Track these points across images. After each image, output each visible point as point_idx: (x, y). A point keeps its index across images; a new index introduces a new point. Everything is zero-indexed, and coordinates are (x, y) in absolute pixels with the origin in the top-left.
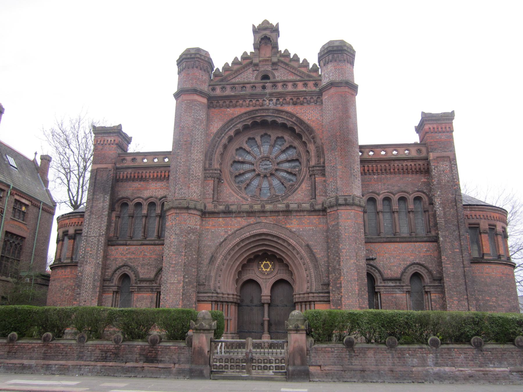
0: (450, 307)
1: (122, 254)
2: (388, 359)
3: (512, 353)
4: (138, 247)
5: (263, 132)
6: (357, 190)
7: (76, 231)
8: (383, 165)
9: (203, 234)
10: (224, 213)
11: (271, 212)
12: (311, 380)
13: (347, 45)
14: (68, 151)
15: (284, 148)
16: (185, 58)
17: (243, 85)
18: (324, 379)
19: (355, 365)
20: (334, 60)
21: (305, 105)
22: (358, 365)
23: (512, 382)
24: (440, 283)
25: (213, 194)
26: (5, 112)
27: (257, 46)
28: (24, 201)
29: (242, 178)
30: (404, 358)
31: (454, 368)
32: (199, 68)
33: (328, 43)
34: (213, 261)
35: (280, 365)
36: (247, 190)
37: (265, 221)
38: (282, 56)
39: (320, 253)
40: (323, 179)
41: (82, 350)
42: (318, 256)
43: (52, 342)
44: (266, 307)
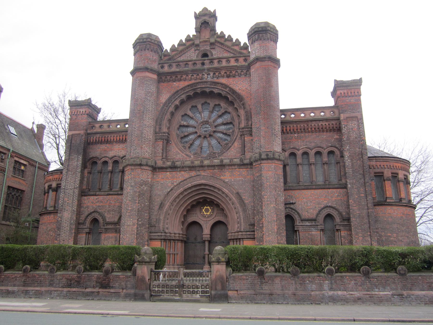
0: (356, 242)
1: (92, 202)
2: (291, 285)
3: (394, 280)
4: (105, 197)
5: (203, 101)
6: (278, 148)
7: (57, 185)
8: (302, 125)
9: (154, 185)
10: (171, 168)
11: (208, 166)
12: (229, 302)
13: (271, 26)
14: (57, 120)
15: (220, 113)
16: (139, 43)
17: (186, 63)
18: (239, 301)
19: (265, 290)
20: (259, 39)
21: (237, 77)
22: (267, 290)
23: (394, 304)
24: (349, 222)
25: (163, 153)
26: (4, 91)
27: (199, 30)
28: (22, 161)
29: (186, 139)
30: (305, 284)
31: (345, 292)
32: (150, 50)
33: (255, 25)
34: (162, 207)
35: (205, 290)
36: (191, 149)
37: (204, 174)
38: (219, 37)
39: (247, 198)
40: (251, 138)
41: (52, 279)
42: (246, 202)
43: (30, 273)
44: (207, 244)
